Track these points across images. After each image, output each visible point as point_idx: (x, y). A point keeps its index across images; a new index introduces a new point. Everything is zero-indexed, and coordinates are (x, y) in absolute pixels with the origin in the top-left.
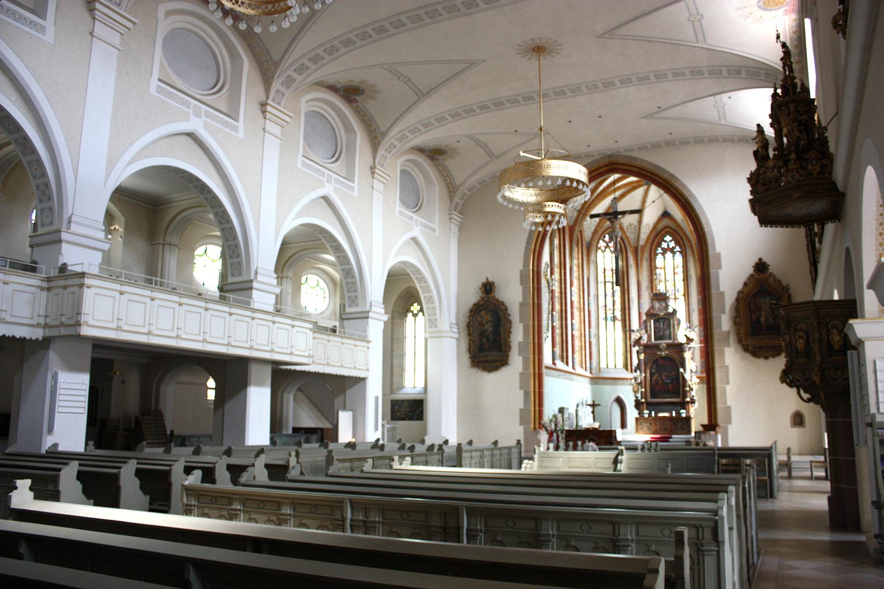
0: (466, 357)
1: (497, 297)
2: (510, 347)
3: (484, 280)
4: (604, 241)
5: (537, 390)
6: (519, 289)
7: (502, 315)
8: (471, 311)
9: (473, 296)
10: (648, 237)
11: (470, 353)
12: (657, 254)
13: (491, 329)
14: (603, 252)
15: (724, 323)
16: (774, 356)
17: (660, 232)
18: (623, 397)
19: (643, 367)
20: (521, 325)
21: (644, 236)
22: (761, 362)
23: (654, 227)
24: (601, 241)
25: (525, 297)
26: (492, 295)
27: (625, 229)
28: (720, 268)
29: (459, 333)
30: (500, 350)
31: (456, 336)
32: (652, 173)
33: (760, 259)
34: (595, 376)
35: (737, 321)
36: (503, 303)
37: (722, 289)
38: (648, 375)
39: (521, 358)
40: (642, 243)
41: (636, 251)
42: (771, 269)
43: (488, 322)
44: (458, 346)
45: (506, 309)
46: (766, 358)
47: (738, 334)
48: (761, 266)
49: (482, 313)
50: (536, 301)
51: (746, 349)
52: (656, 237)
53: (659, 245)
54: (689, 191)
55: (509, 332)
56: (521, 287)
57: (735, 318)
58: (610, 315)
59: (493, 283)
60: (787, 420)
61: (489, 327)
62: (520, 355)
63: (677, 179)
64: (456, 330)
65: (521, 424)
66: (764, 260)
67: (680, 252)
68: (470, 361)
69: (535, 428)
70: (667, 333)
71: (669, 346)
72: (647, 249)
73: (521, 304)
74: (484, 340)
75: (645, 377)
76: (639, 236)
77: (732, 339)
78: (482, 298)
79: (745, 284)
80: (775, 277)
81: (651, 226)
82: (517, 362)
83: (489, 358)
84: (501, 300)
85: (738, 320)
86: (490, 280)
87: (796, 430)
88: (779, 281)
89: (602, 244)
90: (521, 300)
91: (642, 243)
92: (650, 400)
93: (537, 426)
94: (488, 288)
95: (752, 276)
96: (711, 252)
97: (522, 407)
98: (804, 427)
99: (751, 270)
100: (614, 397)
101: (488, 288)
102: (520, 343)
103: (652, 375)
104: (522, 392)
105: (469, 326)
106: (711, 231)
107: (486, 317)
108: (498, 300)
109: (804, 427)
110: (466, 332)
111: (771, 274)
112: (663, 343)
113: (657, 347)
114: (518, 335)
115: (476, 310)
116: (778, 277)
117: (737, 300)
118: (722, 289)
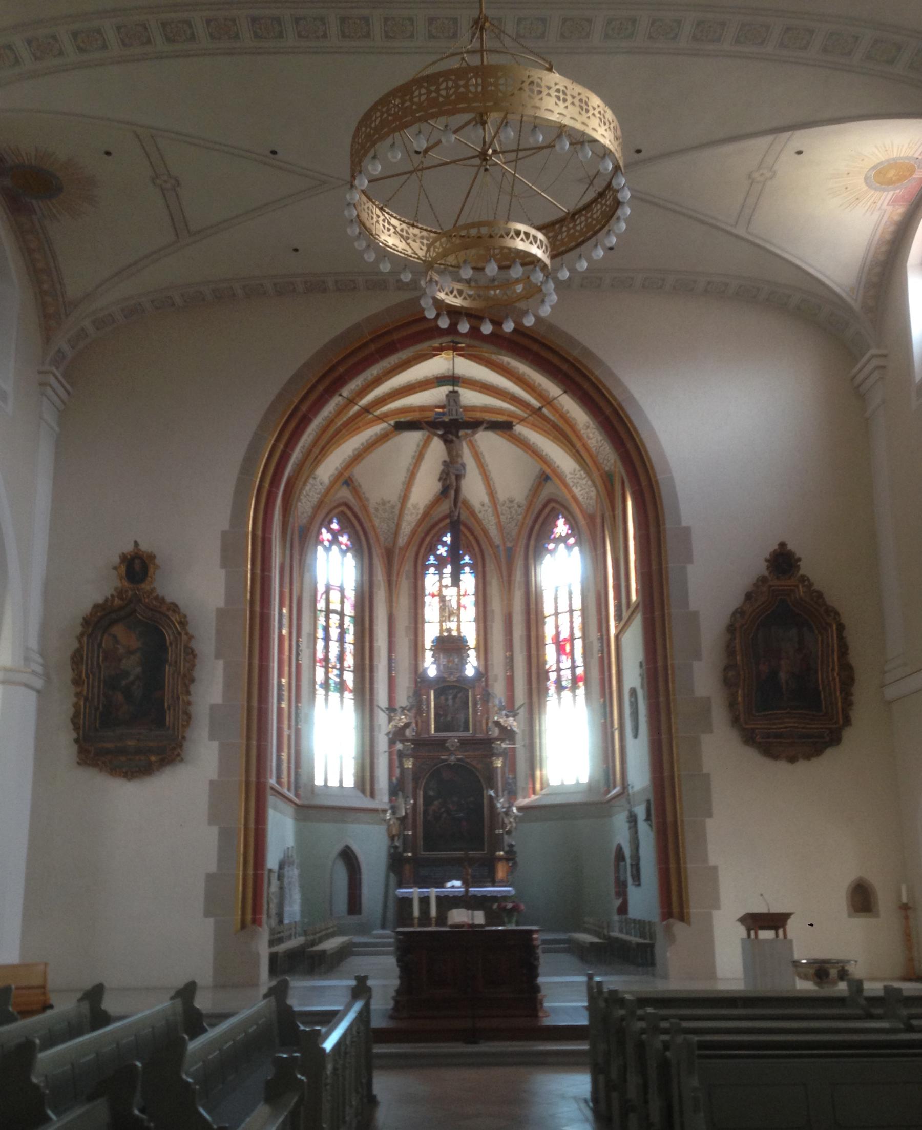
0: (65, 743)
1: (160, 592)
2: (188, 717)
3: (129, 548)
4: (330, 530)
5: (252, 825)
6: (219, 577)
7: (169, 637)
8: (86, 622)
9: (94, 586)
10: (414, 532)
11: (76, 727)
12: (427, 568)
13: (139, 670)
14: (327, 550)
15: (703, 678)
16: (808, 757)
17: (437, 524)
18: (355, 847)
19: (410, 786)
20: (220, 663)
21: (406, 529)
22: (782, 767)
23: (426, 515)
24: (324, 531)
25: (230, 596)
26: (145, 586)
27: (372, 511)
28: (689, 559)
29: (47, 677)
30: (160, 722)
31: (39, 683)
32: (543, 345)
33: (782, 545)
34: (306, 802)
35: (730, 678)
36: (174, 607)
37: (693, 607)
38: (421, 801)
39: (215, 744)
40: (402, 541)
41: (389, 555)
42: (805, 569)
43: (130, 653)
44: (41, 712)
45: (183, 623)
46: (792, 760)
47: (732, 705)
48: (783, 561)
49: (118, 630)
50: (257, 609)
51: (749, 738)
52: (427, 534)
53: (432, 549)
54: (626, 390)
55: (188, 679)
56: (222, 573)
57: (726, 669)
58: (334, 619)
59: (152, 557)
60: (840, 901)
61: (132, 666)
62: (212, 737)
63: (600, 363)
64: (39, 669)
65: (207, 914)
66: (790, 547)
67: (472, 567)
68: (75, 748)
69: (243, 926)
70: (461, 717)
71: (464, 743)
72: (410, 554)
73: (221, 614)
74: (119, 697)
75: (415, 804)
76: (398, 526)
77: (719, 715)
78: (120, 593)
79: (749, 596)
80: (811, 585)
81: (421, 512)
82: (205, 759)
83: (131, 743)
84: (169, 599)
85: (731, 674)
86: (144, 547)
87: (860, 923)
88: (820, 595)
89: (326, 535)
90: (220, 603)
91: (402, 541)
92: (423, 853)
93: (249, 917)
94: (137, 567)
95: (763, 580)
96: (669, 525)
97: (213, 868)
98: (877, 915)
99: (760, 568)
100: (339, 847)
101: (137, 567)
102: (213, 707)
103: (428, 801)
104: (215, 830)
105: (77, 659)
106: (671, 479)
107: (126, 638)
108: (162, 600)
109: (877, 915)
110: (69, 675)
111: (803, 579)
112: (454, 737)
113: (440, 744)
114: (211, 688)
115: (99, 621)
116: (817, 586)
117: (731, 629)
118: (693, 607)
